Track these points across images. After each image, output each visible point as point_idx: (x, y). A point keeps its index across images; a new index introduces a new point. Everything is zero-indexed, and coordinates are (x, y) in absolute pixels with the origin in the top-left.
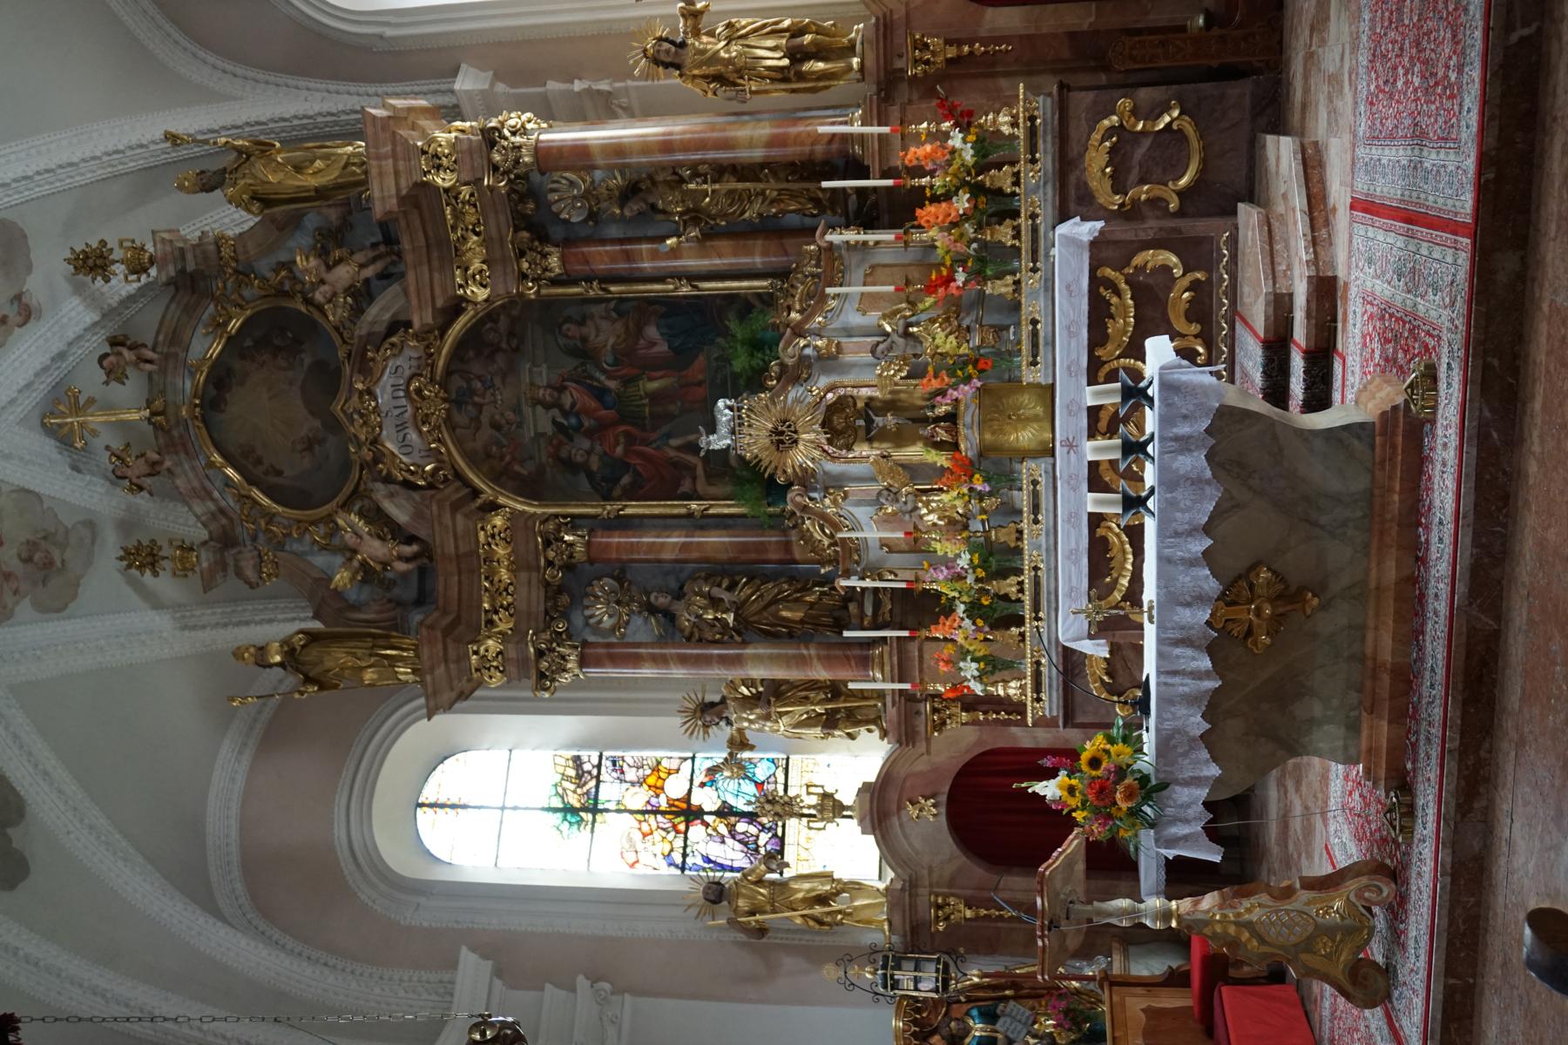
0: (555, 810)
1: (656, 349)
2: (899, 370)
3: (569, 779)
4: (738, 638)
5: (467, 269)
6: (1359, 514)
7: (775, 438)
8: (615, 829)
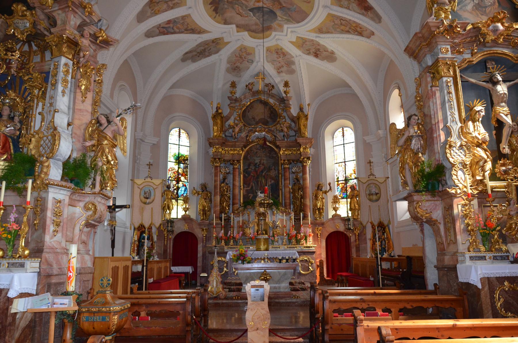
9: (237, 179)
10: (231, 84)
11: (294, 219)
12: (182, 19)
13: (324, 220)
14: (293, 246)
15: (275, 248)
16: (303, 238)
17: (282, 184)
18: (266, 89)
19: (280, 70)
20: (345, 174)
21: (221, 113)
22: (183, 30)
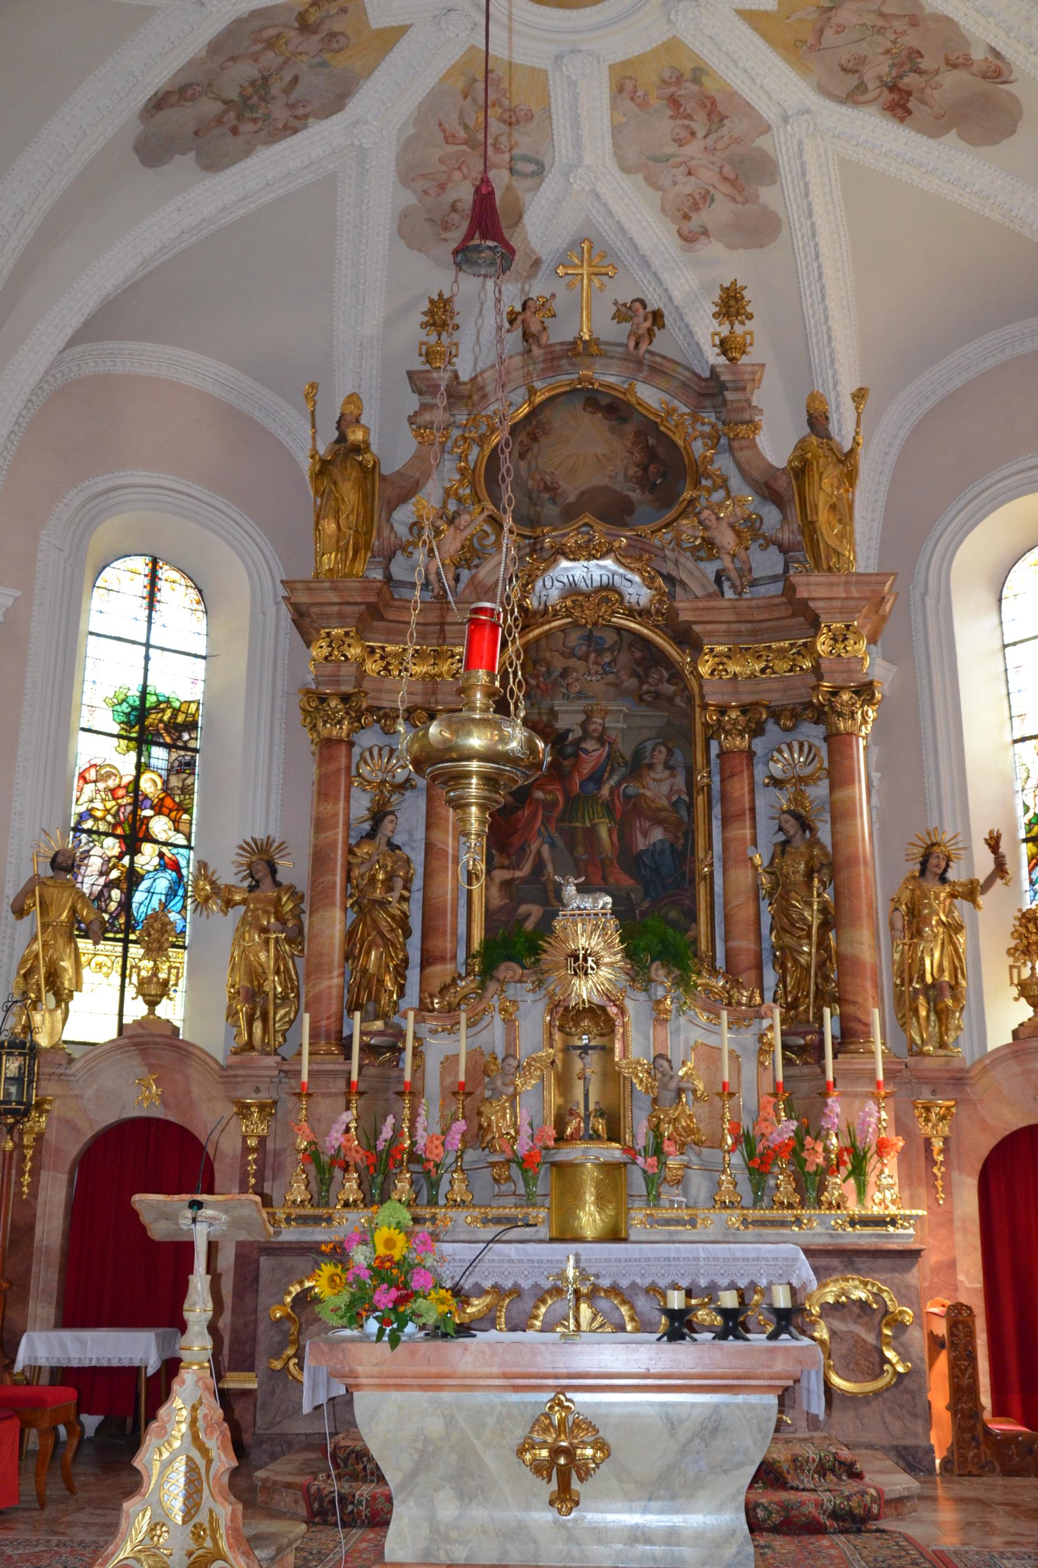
1: (639, 837)
2: (641, 1081)
3: (174, 715)
4: (350, 902)
5: (729, 657)
10: (430, 313)
11: (785, 1047)
13: (964, 1053)
14: (777, 1214)
16: (840, 1162)
17: (710, 846)
19: (698, 220)
21: (358, 449)
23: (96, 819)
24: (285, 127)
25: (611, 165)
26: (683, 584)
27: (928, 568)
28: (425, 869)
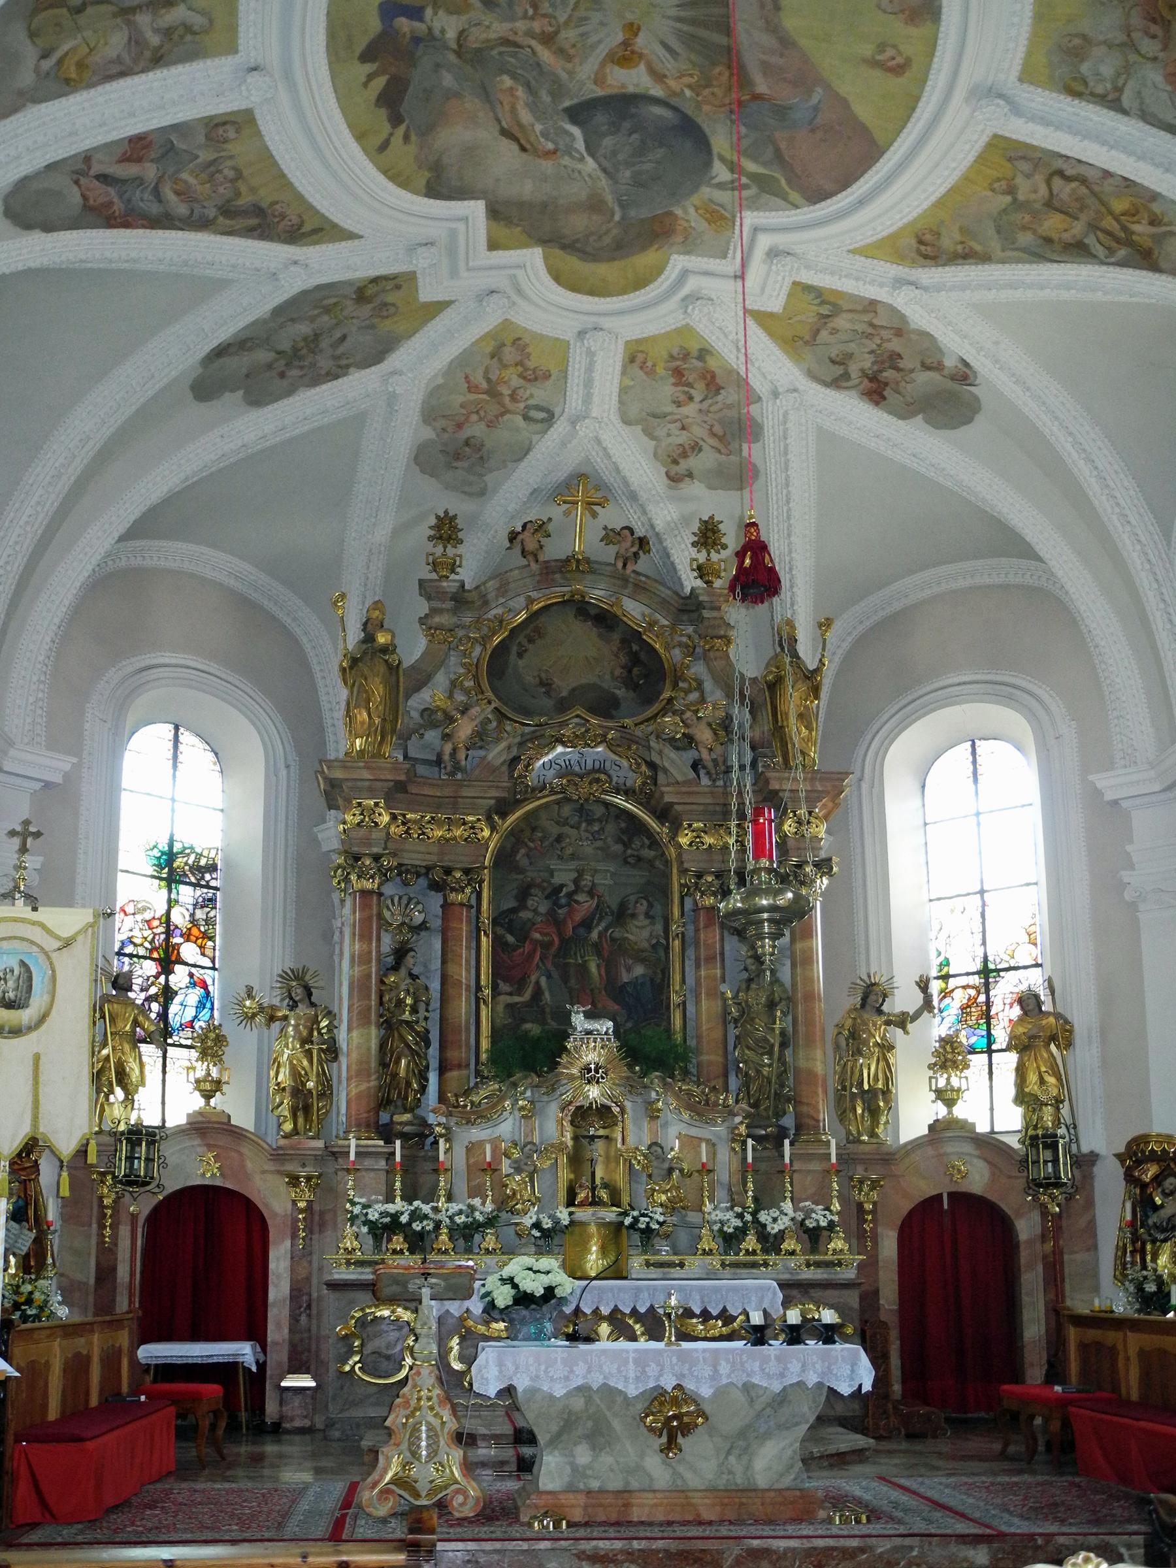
0: (171, 846)
1: (623, 970)
3: (197, 859)
5: (705, 832)
6: (739, 1481)
7: (593, 1066)
8: (156, 897)
9: (464, 952)
10: (438, 527)
12: (208, 137)
15: (661, 1265)
17: (683, 981)
18: (608, 553)
19: (684, 465)
20: (984, 943)
22: (211, 212)
23: (135, 945)
24: (328, 374)
25: (615, 418)
26: (665, 771)
27: (864, 761)
28: (442, 994)
